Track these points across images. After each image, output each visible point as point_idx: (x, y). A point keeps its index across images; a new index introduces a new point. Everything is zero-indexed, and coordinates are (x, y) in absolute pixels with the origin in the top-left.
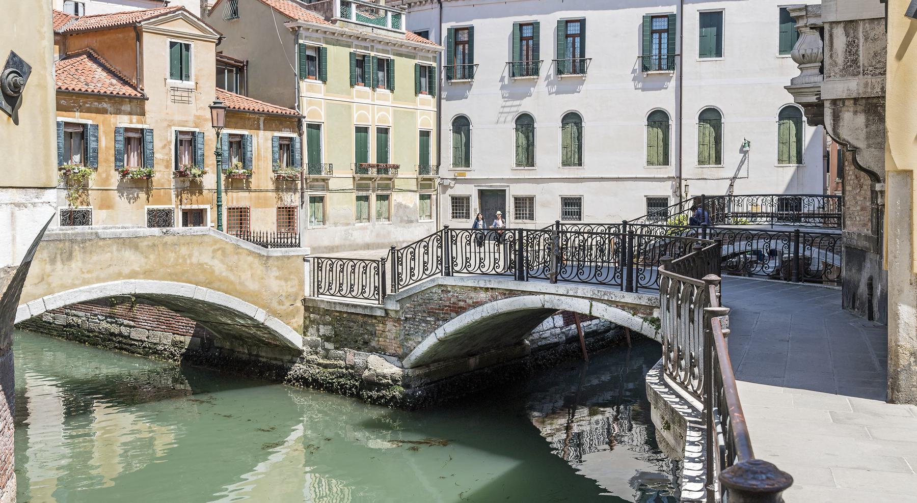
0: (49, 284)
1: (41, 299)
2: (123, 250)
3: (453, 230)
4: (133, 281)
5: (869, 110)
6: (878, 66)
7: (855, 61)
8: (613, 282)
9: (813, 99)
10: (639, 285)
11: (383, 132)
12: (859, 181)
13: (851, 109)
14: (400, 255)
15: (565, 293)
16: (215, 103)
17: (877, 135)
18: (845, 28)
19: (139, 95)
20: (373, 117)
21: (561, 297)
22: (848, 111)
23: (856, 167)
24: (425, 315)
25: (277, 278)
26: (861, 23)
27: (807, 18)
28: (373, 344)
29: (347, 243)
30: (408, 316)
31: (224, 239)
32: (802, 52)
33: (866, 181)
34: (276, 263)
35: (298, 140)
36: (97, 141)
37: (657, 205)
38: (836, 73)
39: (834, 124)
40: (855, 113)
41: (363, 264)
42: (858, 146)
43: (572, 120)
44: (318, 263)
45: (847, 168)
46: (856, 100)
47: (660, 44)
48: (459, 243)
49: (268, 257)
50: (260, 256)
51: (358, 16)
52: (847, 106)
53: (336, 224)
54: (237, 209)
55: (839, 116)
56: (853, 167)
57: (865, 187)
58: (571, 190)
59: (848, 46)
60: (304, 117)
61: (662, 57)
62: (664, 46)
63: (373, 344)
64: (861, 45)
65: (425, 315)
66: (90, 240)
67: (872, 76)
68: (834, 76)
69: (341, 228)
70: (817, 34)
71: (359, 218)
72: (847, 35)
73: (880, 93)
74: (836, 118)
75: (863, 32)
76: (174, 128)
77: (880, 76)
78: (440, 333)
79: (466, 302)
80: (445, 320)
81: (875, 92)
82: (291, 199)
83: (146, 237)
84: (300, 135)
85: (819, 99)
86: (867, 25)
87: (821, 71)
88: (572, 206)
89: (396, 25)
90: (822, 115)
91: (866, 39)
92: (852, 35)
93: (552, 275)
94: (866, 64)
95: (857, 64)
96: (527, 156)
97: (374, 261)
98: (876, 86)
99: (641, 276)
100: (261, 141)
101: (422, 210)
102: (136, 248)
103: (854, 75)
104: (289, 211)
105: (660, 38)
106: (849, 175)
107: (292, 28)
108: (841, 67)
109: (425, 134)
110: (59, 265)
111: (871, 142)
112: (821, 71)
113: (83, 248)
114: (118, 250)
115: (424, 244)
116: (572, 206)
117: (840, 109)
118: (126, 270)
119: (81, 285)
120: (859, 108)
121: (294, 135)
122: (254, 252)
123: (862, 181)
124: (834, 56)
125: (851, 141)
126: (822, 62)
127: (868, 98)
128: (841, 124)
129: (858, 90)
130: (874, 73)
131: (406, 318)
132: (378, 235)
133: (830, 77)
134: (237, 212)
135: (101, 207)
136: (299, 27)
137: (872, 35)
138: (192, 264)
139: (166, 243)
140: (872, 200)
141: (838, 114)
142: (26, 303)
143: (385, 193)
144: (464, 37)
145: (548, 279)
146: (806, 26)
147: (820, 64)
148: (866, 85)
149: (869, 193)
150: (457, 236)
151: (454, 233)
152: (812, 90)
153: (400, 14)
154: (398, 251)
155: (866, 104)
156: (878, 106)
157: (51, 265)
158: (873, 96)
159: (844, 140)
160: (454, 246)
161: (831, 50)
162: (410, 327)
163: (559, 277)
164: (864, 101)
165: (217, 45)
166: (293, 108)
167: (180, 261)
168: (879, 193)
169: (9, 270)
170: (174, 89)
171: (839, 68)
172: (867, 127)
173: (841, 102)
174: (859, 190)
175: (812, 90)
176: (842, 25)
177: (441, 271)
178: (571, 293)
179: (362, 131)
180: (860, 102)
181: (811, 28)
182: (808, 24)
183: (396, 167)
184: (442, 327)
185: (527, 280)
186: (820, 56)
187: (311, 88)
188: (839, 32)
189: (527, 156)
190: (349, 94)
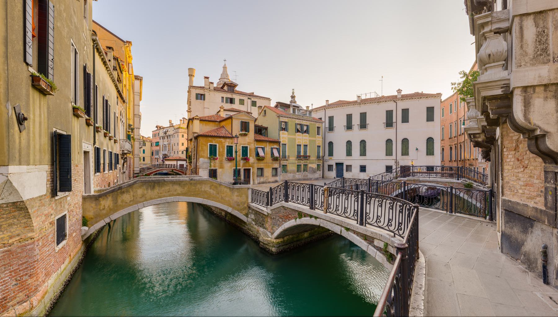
0: (146, 198)
4: (178, 197)
10: (367, 222)
13: (542, 96)
15: (329, 220)
18: (534, 19)
20: (303, 142)
21: (328, 222)
22: (539, 97)
25: (237, 196)
37: (389, 169)
38: (527, 63)
39: (525, 110)
40: (546, 98)
42: (549, 130)
43: (363, 143)
46: (546, 86)
48: (290, 189)
53: (290, 173)
55: (529, 103)
58: (363, 163)
59: (538, 36)
64: (550, 34)
68: (525, 65)
69: (292, 174)
71: (298, 171)
72: (537, 26)
74: (527, 104)
75: (552, 22)
76: (242, 146)
80: (285, 222)
84: (280, 147)
88: (363, 169)
93: (324, 209)
95: (547, 52)
96: (349, 153)
99: (368, 217)
100: (268, 149)
102: (180, 184)
103: (544, 63)
106: (508, 158)
108: (531, 57)
110: (149, 191)
114: (172, 186)
117: (530, 96)
118: (175, 193)
119: (158, 198)
120: (550, 94)
124: (525, 46)
125: (542, 126)
128: (532, 110)
129: (549, 76)
132: (304, 176)
133: (521, 66)
135: (220, 168)
138: (201, 191)
143: (306, 164)
145: (323, 210)
152: (499, 83)
171: (529, 58)
173: (532, 89)
175: (499, 83)
176: (532, 17)
179: (299, 146)
180: (550, 88)
181: (495, 33)
187: (283, 134)
188: (529, 23)
189: (349, 153)
190: (295, 135)
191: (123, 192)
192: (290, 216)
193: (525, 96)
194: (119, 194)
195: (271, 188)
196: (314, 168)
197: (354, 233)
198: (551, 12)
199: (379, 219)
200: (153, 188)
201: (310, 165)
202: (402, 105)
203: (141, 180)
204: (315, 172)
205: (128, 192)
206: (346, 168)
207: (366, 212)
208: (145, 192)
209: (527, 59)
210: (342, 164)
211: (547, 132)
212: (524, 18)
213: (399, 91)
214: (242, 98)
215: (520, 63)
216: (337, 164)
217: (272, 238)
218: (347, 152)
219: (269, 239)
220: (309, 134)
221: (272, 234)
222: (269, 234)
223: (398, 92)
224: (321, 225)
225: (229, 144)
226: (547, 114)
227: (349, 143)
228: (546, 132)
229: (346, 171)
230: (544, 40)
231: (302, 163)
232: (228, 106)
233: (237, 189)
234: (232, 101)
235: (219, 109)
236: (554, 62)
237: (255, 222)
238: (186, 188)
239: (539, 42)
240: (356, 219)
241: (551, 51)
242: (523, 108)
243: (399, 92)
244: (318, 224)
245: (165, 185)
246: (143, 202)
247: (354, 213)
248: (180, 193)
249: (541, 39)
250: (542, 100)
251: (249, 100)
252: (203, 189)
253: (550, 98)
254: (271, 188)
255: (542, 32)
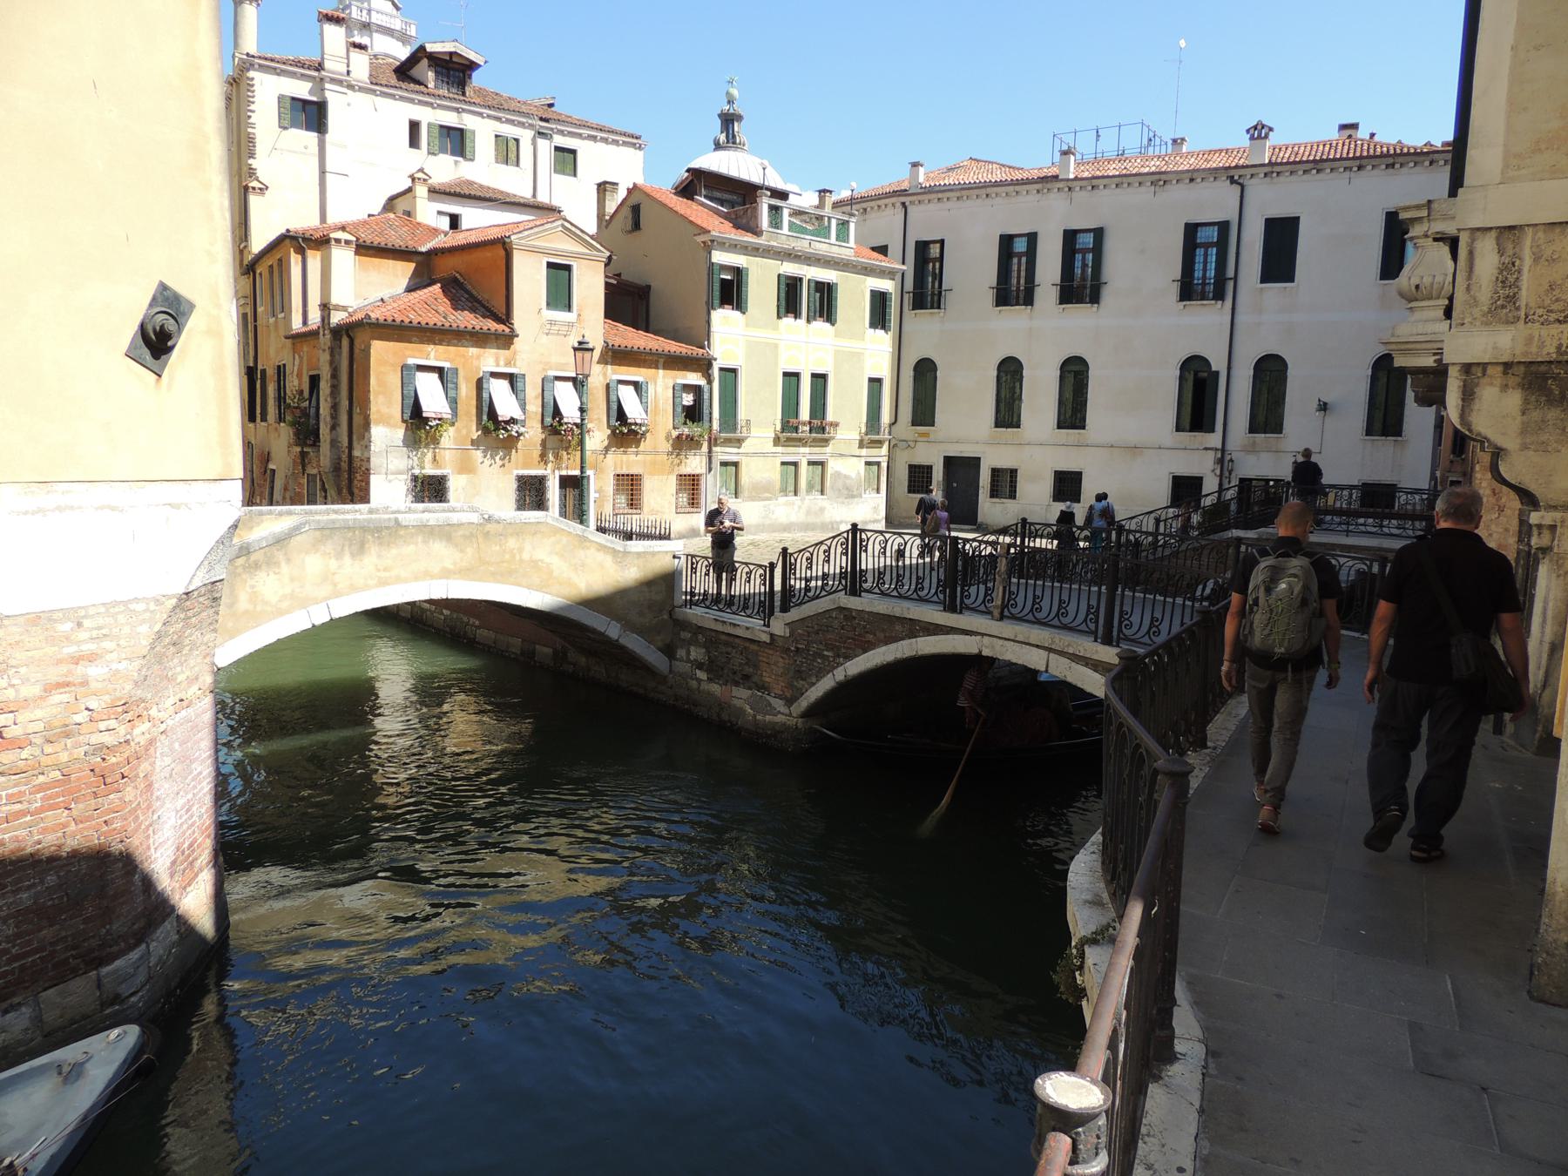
1: (325, 604)
2: (431, 541)
3: (864, 531)
5: (1530, 384)
6: (1554, 307)
7: (1512, 299)
8: (1083, 627)
9: (1429, 361)
11: (820, 379)
12: (1497, 500)
13: (1498, 382)
14: (793, 561)
15: (1012, 638)
16: (580, 343)
17: (1540, 429)
18: (1498, 239)
19: (507, 330)
21: (1006, 642)
22: (1491, 384)
23: (1493, 477)
24: (821, 647)
26: (1530, 232)
27: (1429, 221)
28: (755, 679)
29: (768, 522)
30: (800, 646)
31: (566, 528)
32: (1415, 281)
33: (1513, 503)
34: (636, 562)
35: (706, 389)
36: (456, 388)
38: (1475, 319)
39: (1463, 406)
40: (1505, 388)
41: (746, 570)
42: (1504, 446)
43: (1074, 374)
44: (692, 564)
45: (1478, 475)
46: (1507, 366)
47: (1205, 262)
49: (626, 553)
50: (615, 552)
51: (791, 225)
52: (1491, 377)
54: (628, 475)
56: (1489, 475)
57: (1508, 512)
59: (1501, 272)
60: (715, 359)
61: (1207, 281)
62: (1212, 266)
63: (755, 679)
65: (821, 647)
66: (387, 528)
67: (1542, 324)
68: (1471, 323)
70: (1445, 250)
71: (784, 491)
72: (1501, 252)
73: (1554, 356)
74: (1468, 395)
75: (1531, 248)
77: (1557, 325)
78: (840, 674)
79: (875, 635)
80: (848, 658)
81: (1545, 352)
82: (694, 463)
83: (462, 524)
84: (710, 382)
85: (1439, 361)
86: (1540, 234)
87: (1448, 313)
89: (843, 235)
90: (1443, 389)
91: (1537, 259)
92: (1511, 253)
94: (1532, 304)
95: (1514, 303)
96: (1007, 414)
97: (760, 566)
98: (1548, 343)
99: (1126, 622)
100: (659, 390)
101: (868, 479)
103: (1508, 322)
104: (693, 480)
105: (1206, 255)
107: (704, 242)
108: (1485, 309)
109: (875, 382)
110: (347, 559)
111: (1528, 441)
112: (1448, 313)
113: (379, 537)
115: (824, 547)
116: (1067, 485)
120: (1512, 381)
121: (702, 382)
122: (606, 547)
123: (1503, 500)
124: (1474, 288)
126: (1451, 299)
127: (1530, 362)
130: (1546, 320)
131: (797, 649)
132: (808, 513)
133: (1463, 324)
134: (627, 480)
136: (712, 241)
137: (1548, 253)
138: (521, 561)
139: (488, 532)
140: (1520, 537)
141: (1472, 390)
142: (305, 608)
144: (934, 251)
146: (1426, 236)
147: (1447, 302)
148: (1530, 339)
149: (1515, 523)
150: (868, 539)
151: (864, 536)
153: (848, 222)
154: (791, 554)
155: (1525, 374)
156: (1548, 379)
157: (337, 559)
158: (1539, 360)
159: (1479, 434)
160: (864, 555)
161: (1469, 277)
162: (802, 663)
163: (1006, 613)
164: (1522, 368)
165: (606, 265)
166: (703, 348)
167: (507, 557)
168: (1534, 529)
169: (164, 599)
170: (552, 323)
172: (1523, 414)
174: (1497, 515)
176: (1494, 234)
177: (845, 588)
178: (1020, 638)
179: (792, 377)
180: (1515, 369)
181: (1436, 240)
182: (1429, 233)
183: (835, 425)
184: (842, 668)
185: (961, 613)
186: (1448, 288)
189: (1007, 414)
191: (257, 566)
192: (870, 637)
193: (1465, 381)
194: (240, 570)
195: (785, 550)
196: (853, 475)
197: (1086, 665)
198: (1531, 229)
199: (1157, 627)
200: (360, 549)
201: (833, 466)
202: (1268, 201)
203: (319, 521)
204: (853, 497)
205: (271, 563)
206: (993, 481)
207: (1121, 611)
208: (333, 564)
209: (1477, 312)
210: (974, 463)
211: (1502, 449)
212: (1479, 233)
213: (1259, 132)
214: (509, 131)
215: (1463, 319)
216: (949, 461)
217: (790, 715)
218: (998, 411)
219: (780, 718)
220: (833, 325)
221: (790, 702)
222: (778, 704)
223: (1252, 138)
224: (984, 654)
225: (498, 365)
226: (1504, 417)
227: (1010, 371)
228: (1498, 448)
229: (992, 496)
230: (1511, 279)
231: (803, 454)
232: (445, 169)
233: (639, 554)
234: (456, 141)
235: (409, 183)
236: (1526, 323)
237: (709, 671)
238: (469, 550)
239: (1503, 282)
240: (1093, 629)
241: (1522, 303)
242: (1460, 403)
243: (1260, 137)
244: (975, 651)
245: (401, 537)
246: (326, 599)
247: (1087, 615)
248: (451, 567)
249: (1506, 278)
250: (1497, 389)
251: (543, 144)
252: (526, 556)
253: (1513, 388)
254: (785, 550)
255: (1510, 265)
